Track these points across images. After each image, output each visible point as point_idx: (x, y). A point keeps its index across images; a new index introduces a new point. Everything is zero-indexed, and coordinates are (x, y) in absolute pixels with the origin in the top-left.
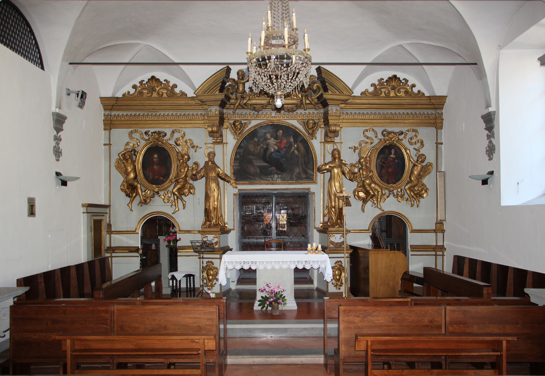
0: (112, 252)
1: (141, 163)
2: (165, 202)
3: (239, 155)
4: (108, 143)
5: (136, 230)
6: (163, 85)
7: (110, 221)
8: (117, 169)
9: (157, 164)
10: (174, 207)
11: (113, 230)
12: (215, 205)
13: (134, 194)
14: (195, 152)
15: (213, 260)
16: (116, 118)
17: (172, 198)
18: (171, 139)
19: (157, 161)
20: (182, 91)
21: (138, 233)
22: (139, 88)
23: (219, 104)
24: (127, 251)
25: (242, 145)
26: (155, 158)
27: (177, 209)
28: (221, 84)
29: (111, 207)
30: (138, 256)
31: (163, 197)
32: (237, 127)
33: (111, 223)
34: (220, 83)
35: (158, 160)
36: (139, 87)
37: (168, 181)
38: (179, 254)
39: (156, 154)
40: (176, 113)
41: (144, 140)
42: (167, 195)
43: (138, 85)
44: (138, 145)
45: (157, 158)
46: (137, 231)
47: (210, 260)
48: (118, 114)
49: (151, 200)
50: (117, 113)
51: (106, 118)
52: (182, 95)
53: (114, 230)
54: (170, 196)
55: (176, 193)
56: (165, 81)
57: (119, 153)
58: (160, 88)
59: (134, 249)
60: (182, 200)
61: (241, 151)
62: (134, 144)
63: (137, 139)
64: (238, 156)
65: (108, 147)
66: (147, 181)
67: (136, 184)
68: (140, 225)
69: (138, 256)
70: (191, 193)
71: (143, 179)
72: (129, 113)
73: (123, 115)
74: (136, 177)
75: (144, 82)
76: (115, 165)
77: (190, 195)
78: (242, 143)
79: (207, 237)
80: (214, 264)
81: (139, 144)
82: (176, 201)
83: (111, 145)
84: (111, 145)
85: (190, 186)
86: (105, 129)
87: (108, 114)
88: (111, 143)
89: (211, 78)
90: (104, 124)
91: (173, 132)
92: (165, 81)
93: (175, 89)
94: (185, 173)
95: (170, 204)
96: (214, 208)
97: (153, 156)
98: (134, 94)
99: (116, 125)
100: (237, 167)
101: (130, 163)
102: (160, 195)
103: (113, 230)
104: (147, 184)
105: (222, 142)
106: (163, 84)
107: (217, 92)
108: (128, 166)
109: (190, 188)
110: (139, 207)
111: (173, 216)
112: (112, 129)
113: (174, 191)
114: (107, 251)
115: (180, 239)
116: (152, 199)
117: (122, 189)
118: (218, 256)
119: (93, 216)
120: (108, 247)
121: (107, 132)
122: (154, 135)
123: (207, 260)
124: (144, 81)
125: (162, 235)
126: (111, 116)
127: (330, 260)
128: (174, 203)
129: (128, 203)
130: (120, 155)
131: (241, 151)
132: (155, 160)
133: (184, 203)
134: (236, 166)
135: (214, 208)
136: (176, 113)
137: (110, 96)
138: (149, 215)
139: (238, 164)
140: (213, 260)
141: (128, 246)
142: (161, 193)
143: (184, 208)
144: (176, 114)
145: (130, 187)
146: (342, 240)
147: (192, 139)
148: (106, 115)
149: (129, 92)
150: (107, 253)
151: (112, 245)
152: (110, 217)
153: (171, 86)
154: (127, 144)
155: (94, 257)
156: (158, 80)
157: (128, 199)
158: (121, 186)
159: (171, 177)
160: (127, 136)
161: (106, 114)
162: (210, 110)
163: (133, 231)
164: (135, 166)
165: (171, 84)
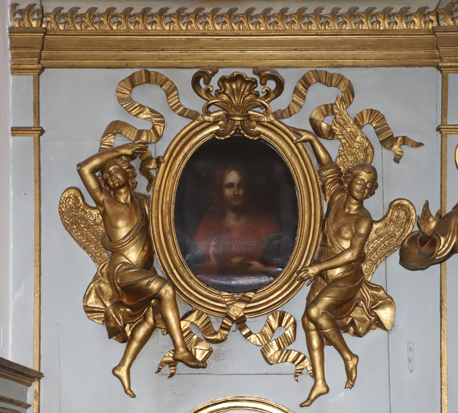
1: (173, 207)
4: (30, 123)
14: (397, 160)
19: (236, 197)
26: (231, 185)
27: (320, 388)
35: (241, 192)
39: (237, 170)
45: (239, 185)
55: (323, 322)
70: (379, 323)
83: (42, 132)
84: (42, 132)
86: (15, 70)
97: (223, 178)
102: (250, 333)
116: (214, 347)
121: (28, 79)
130: (86, 170)
132: (228, 192)
148: (21, 12)
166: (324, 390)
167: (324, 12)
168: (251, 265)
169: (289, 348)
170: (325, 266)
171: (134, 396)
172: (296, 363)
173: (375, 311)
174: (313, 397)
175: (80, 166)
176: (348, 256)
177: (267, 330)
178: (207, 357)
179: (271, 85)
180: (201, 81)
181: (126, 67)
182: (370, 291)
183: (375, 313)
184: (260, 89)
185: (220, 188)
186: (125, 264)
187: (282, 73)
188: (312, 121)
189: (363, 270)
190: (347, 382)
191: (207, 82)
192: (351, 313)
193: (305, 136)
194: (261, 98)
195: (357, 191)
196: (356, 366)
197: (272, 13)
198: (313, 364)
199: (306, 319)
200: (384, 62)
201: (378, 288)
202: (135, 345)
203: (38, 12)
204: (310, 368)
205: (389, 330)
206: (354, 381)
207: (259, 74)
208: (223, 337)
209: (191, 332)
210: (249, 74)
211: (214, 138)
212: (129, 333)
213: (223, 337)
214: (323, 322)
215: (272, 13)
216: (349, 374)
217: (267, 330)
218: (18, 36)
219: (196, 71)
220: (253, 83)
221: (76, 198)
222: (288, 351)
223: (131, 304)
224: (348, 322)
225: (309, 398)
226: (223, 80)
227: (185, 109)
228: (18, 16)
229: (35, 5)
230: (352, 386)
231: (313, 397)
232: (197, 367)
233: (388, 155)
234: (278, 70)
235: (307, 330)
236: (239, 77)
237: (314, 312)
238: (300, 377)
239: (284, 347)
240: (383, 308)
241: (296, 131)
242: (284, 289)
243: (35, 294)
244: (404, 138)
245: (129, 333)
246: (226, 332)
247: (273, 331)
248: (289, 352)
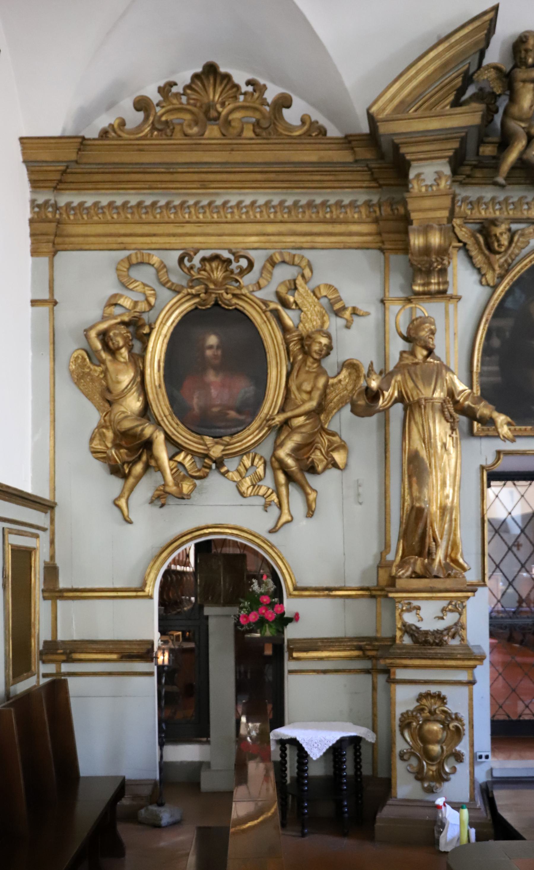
0: (64, 657)
1: (162, 364)
2: (242, 494)
3: (498, 336)
4: (46, 296)
5: (145, 584)
6: (242, 98)
7: (52, 557)
8: (77, 383)
9: (217, 369)
10: (274, 510)
11: (62, 585)
12: (447, 497)
13: (139, 468)
14: (348, 327)
15: (444, 690)
16: (75, 214)
17: (268, 482)
18: (263, 282)
19: (215, 356)
20: (310, 117)
21: (151, 597)
22: (158, 109)
23: (450, 153)
24: (114, 656)
25: (509, 304)
26: (211, 347)
27: (285, 517)
28: (460, 79)
29: (57, 509)
30: (151, 674)
31: (237, 478)
32: (498, 241)
33: (58, 562)
34: (457, 77)
35: (219, 352)
36: (158, 105)
37: (255, 424)
38: (289, 665)
39: (216, 334)
40: (283, 197)
41: (169, 288)
42: (251, 472)
43: (155, 97)
44: (149, 303)
45: (218, 347)
46: (147, 589)
47: (434, 689)
48: (81, 204)
49: (195, 486)
50: (76, 199)
51: (38, 213)
52: (307, 134)
53: (69, 586)
54: (262, 473)
55: (290, 462)
56: (248, 83)
57: (87, 327)
58: (231, 106)
59: (136, 649)
60: (303, 487)
61: (507, 323)
62: (136, 303)
63: (145, 285)
64: (496, 343)
65: (45, 310)
66: (183, 423)
67: (148, 430)
68: (159, 571)
69: (151, 674)
70: (335, 465)
71: (170, 418)
72: (119, 201)
73: (96, 204)
74: (146, 406)
75: (174, 90)
76: (71, 373)
77: (333, 473)
78: (510, 299)
79: (419, 608)
80: (446, 703)
81: (152, 300)
82: (283, 490)
83: (55, 303)
84: (55, 303)
85: (329, 441)
86: (35, 252)
87: (46, 202)
88: (57, 298)
89: (432, 54)
90: (32, 235)
91: (272, 262)
92: (248, 83)
93: (285, 111)
94: (316, 394)
95: (262, 501)
96: (443, 509)
97: (204, 340)
98: (139, 128)
99: (73, 239)
100: (492, 379)
101: (125, 363)
102: (228, 471)
103: (62, 585)
104: (184, 433)
105: (444, 292)
106: (245, 94)
107: (448, 107)
108: (118, 372)
109: (332, 448)
110: (155, 510)
111: (273, 538)
112: (60, 254)
113: (282, 453)
114: (44, 658)
115: (296, 618)
116: (197, 482)
117: (94, 452)
118: (463, 676)
119: (11, 532)
120: (46, 642)
121: (45, 260)
122: (208, 267)
123: (423, 689)
124: (175, 84)
125: (216, 603)
126: (56, 207)
127: (154, 637)
128: (274, 497)
129: (116, 494)
130: (93, 334)
131: (507, 323)
132: (209, 353)
133: (312, 496)
134: (490, 374)
135: (443, 509)
136: (283, 197)
137: (57, 133)
138: (189, 537)
139: (496, 368)
140: (444, 690)
141: (116, 638)
142: (231, 465)
143: (310, 512)
144: (282, 203)
145: (123, 443)
146: (451, 619)
147: (336, 286)
148: (39, 206)
149: (123, 123)
150: (44, 662)
151: (60, 637)
152: (52, 542)
153: (270, 100)
154: (113, 302)
155: (13, 677)
156: (227, 77)
157: (116, 483)
158: (92, 440)
159: (265, 411)
160: (112, 277)
161: (41, 200)
162: (418, 176)
163: (136, 591)
164: (143, 374)
165: (270, 96)
166: (290, 518)
167: (287, 204)
168: (228, 414)
169: (260, 483)
170: (289, 414)
171: (130, 522)
172: (265, 496)
173: (331, 453)
174: (279, 525)
175: (87, 331)
176: (308, 406)
177: (242, 469)
178: (192, 491)
179: (244, 263)
180: (186, 259)
181: (125, 249)
182: (328, 436)
183: (331, 455)
184: (234, 265)
185: (202, 348)
186: (123, 412)
187: (252, 254)
188: (277, 294)
189: (501, 419)
190: (308, 513)
191: (190, 260)
192: (311, 454)
193: (272, 306)
194: (236, 274)
195: (315, 352)
196: (315, 500)
197: (244, 204)
198: (279, 497)
199: (273, 459)
200: (337, 245)
201: (334, 434)
202: (131, 480)
203: (52, 206)
204: (276, 500)
205: (490, 493)
206: (313, 512)
207: (234, 254)
208: (205, 475)
209: (178, 470)
210: (226, 255)
211: (196, 308)
212: (127, 471)
213: (205, 475)
214: (290, 462)
215: (244, 204)
216: (309, 507)
217: (242, 469)
218: (36, 225)
219: (181, 252)
220: (229, 261)
221: (83, 359)
222: (259, 486)
223: (129, 446)
224: (308, 463)
225: (276, 525)
226: (204, 260)
227: (173, 284)
228: (36, 209)
229: (50, 200)
230: (312, 515)
231: (279, 525)
232: (183, 498)
233: (341, 322)
234: (394, 138)
235: (274, 470)
236: (216, 258)
237: (282, 453)
238: (269, 509)
239: (256, 483)
240: (338, 451)
241: (265, 303)
242: (255, 434)
243: (50, 437)
244: (354, 309)
245: (127, 471)
246: (207, 470)
247: (247, 470)
248: (260, 487)
